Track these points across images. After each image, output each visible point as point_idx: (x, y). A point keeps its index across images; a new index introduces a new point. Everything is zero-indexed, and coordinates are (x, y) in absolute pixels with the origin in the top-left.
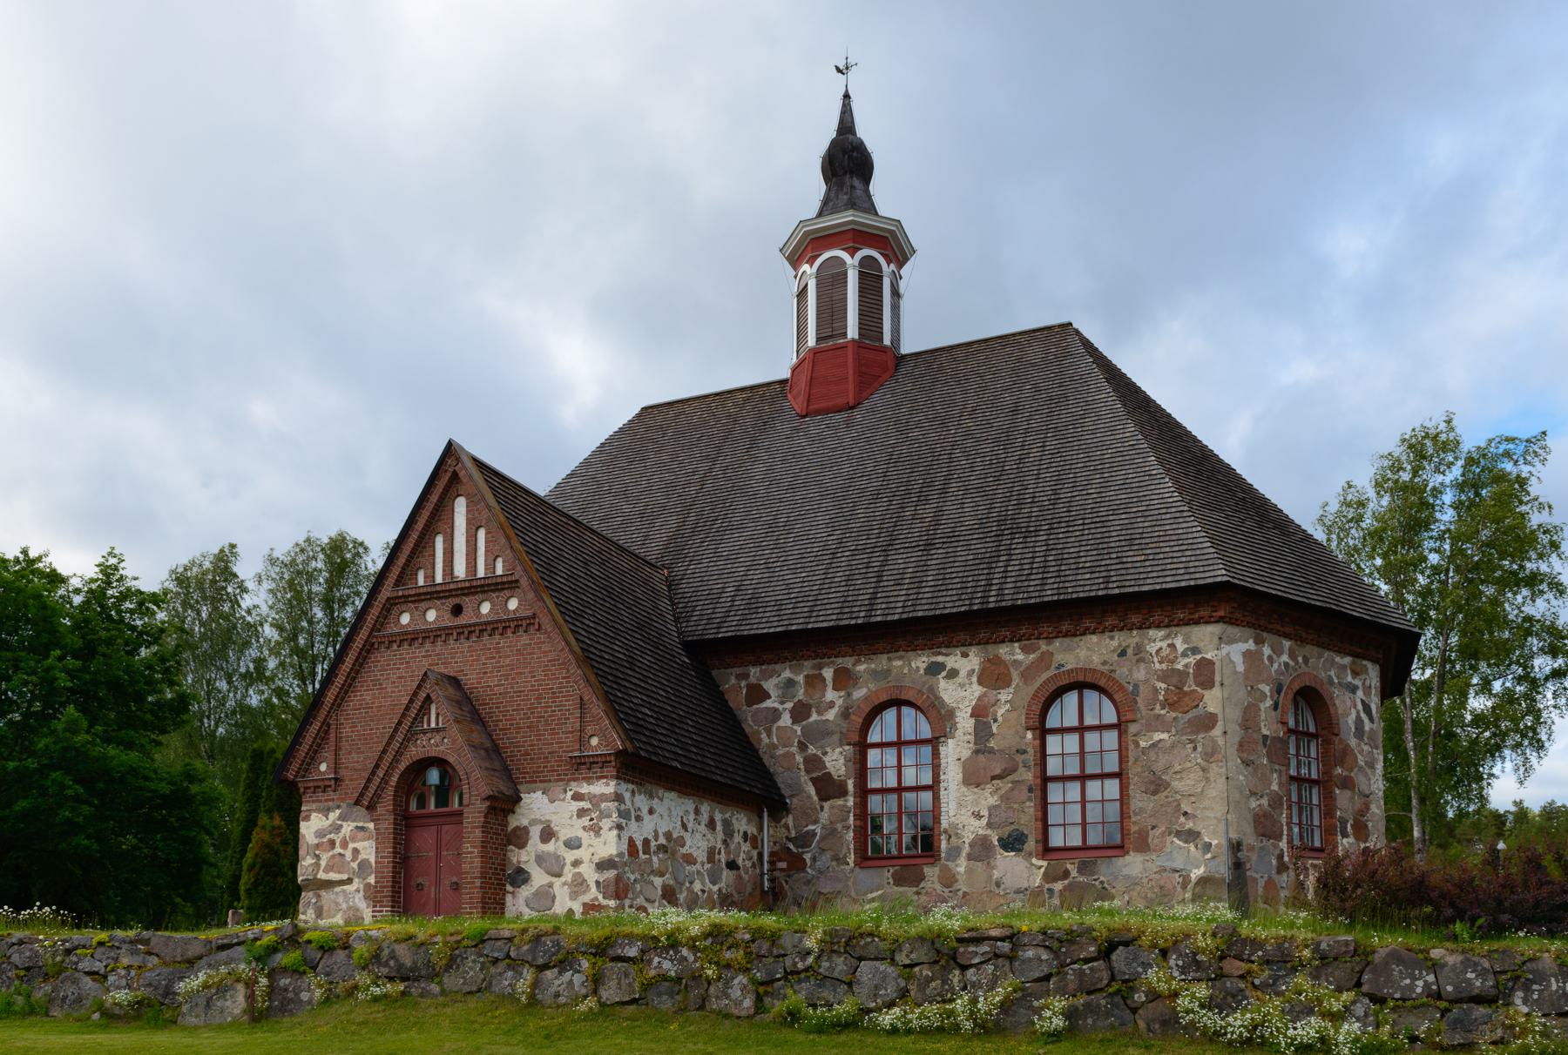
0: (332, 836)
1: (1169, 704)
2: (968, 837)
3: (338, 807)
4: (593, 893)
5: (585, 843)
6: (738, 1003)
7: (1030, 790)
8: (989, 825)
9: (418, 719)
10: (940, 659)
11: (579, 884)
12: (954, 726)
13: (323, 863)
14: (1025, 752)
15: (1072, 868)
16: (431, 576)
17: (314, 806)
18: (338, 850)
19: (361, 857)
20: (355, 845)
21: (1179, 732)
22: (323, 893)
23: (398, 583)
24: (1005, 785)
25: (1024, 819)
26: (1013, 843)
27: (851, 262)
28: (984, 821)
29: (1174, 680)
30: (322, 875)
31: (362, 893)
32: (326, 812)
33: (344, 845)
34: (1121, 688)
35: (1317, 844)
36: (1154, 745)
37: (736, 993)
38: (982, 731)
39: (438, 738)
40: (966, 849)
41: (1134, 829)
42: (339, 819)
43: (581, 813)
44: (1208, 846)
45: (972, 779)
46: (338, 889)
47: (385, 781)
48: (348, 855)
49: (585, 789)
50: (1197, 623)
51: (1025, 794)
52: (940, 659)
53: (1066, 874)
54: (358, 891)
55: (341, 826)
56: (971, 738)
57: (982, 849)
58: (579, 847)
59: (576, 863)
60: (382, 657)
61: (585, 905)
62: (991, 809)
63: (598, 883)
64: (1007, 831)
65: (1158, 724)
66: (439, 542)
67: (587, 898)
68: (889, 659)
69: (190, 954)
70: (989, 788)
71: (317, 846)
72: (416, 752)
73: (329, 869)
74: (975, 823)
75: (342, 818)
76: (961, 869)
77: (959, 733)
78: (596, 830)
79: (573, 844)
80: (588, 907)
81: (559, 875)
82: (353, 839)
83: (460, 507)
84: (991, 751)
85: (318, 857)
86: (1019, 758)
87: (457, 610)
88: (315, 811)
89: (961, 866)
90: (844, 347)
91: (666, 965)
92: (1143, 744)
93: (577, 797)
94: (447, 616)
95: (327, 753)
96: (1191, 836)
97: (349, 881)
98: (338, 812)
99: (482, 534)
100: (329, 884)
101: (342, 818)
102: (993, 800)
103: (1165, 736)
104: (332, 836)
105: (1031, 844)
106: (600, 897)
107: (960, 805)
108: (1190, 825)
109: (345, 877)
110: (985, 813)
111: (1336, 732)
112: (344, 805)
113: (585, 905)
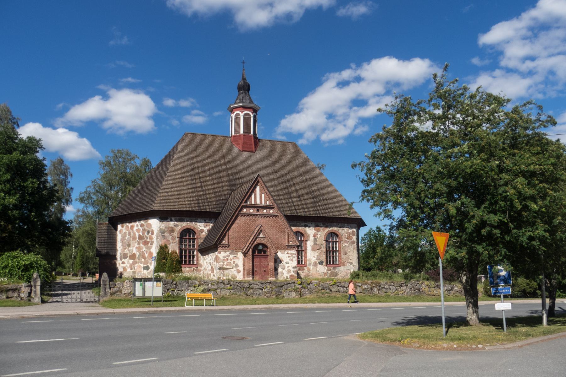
0: (228, 258)
1: (347, 238)
2: (313, 261)
3: (229, 251)
4: (292, 273)
5: (290, 263)
6: (376, 292)
7: (324, 253)
8: (317, 259)
9: (258, 236)
10: (307, 224)
11: (289, 271)
12: (309, 238)
13: (225, 264)
14: (323, 245)
15: (331, 268)
16: (251, 202)
17: (222, 250)
18: (229, 261)
19: (235, 263)
20: (234, 260)
21: (350, 244)
22: (225, 271)
23: (245, 203)
24: (319, 251)
25: (323, 258)
26: (321, 263)
27: (242, 115)
28: (316, 258)
29: (349, 234)
30: (225, 267)
31: (236, 271)
32: (226, 252)
33: (231, 260)
34: (340, 234)
35: (338, 264)
36: (345, 246)
37: (375, 291)
38: (315, 240)
39: (263, 239)
40: (312, 264)
41: (342, 261)
42: (229, 254)
43: (289, 257)
44: (354, 265)
45: (313, 249)
46: (229, 270)
47: (250, 248)
48: (232, 262)
49: (289, 252)
50: (352, 223)
51: (323, 254)
52: (307, 224)
53: (330, 270)
54: (235, 270)
55: (230, 256)
56: (313, 241)
57: (315, 264)
58: (289, 263)
59: (288, 267)
60: (239, 218)
61: (290, 275)
62: (317, 256)
63: (293, 271)
64: (320, 261)
65: (346, 242)
66: (253, 196)
67: (291, 274)
68: (297, 223)
69: (282, 285)
70: (316, 252)
71: (224, 260)
72: (258, 241)
73: (227, 265)
74: (313, 258)
75: (230, 254)
76: (311, 268)
77: (310, 240)
78: (292, 260)
79: (287, 263)
80: (291, 276)
81: (284, 269)
82: (233, 259)
83: (258, 189)
84: (317, 244)
85: (224, 262)
86: (322, 246)
87: (258, 210)
88: (223, 251)
89: (311, 267)
90: (240, 136)
91: (366, 287)
92: (343, 245)
93: (288, 253)
94: (256, 211)
95: (226, 239)
96: (351, 263)
97: (232, 268)
98: (229, 252)
99: (263, 195)
100: (227, 269)
101: (230, 254)
102: (317, 254)
103: (347, 244)
104: (228, 258)
105: (324, 263)
106: (294, 274)
107: (311, 255)
108: (351, 261)
109: (231, 267)
110: (316, 257)
111: (137, 249)
112: (230, 251)
113: (290, 275)
